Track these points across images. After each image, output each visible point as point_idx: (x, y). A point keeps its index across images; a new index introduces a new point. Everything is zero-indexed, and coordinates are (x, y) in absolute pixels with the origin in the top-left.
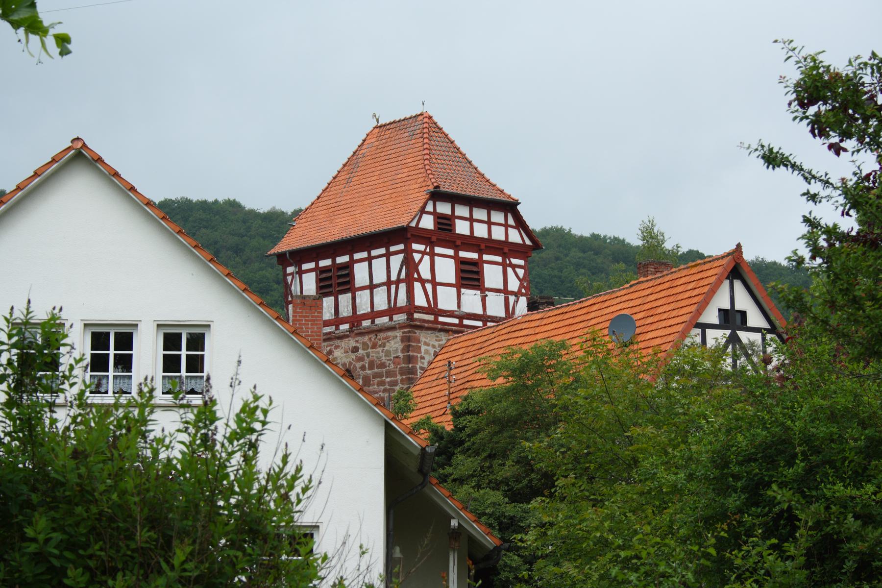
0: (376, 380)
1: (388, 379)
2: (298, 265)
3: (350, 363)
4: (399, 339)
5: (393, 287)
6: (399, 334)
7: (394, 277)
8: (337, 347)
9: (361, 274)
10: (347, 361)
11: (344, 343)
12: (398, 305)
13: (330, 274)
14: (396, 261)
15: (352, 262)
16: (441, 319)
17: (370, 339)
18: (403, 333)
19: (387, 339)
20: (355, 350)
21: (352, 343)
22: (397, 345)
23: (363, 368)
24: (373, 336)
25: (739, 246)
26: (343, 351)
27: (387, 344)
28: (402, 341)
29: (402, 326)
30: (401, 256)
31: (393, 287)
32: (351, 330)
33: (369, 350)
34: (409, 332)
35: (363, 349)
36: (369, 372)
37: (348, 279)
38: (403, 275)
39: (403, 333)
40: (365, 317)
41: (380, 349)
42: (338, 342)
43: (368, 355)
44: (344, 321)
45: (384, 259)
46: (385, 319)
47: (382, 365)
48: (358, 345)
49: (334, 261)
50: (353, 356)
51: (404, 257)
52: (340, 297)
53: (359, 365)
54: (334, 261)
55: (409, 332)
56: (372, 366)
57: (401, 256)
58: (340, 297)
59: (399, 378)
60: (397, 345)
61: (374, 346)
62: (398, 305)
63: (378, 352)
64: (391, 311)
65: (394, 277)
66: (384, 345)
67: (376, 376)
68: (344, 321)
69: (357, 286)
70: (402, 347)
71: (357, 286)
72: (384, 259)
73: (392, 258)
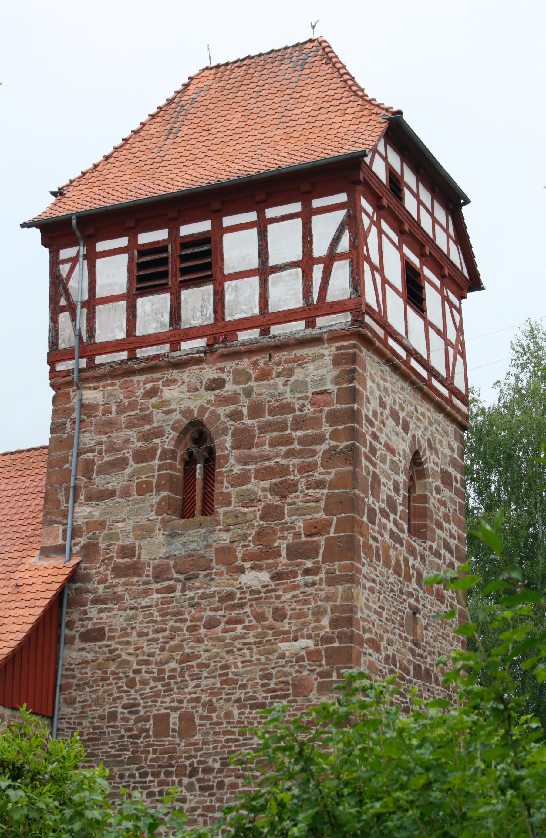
0: (268, 437)
1: (299, 433)
2: (90, 241)
3: (202, 409)
4: (328, 360)
5: (318, 271)
6: (328, 351)
7: (320, 249)
8: (169, 383)
9: (238, 249)
10: (194, 405)
11: (187, 375)
12: (331, 297)
13: (316, 578)
14: (325, 227)
15: (219, 231)
16: (99, 360)
17: (255, 364)
18: (338, 348)
19: (300, 362)
20: (216, 384)
21: (209, 372)
22: (322, 371)
23: (236, 416)
24: (262, 360)
25: (483, 289)
26: (185, 388)
27: (298, 370)
28: (336, 362)
29: (335, 336)
30: (341, 214)
31: (318, 271)
32: (209, 349)
33: (251, 383)
34: (354, 346)
35: (236, 382)
36: (250, 422)
37: (206, 248)
38: (344, 245)
39: (338, 348)
40: (245, 324)
41: (280, 381)
42: (175, 373)
43: (248, 393)
44: (193, 333)
45: (298, 222)
46: (253, 334)
47: (287, 408)
48: (224, 376)
49: (174, 232)
50: (211, 396)
51: (348, 216)
52: (185, 294)
53: (222, 411)
54: (174, 232)
55: (354, 346)
56: (256, 410)
57: (341, 214)
58: (185, 294)
59: (327, 429)
60: (322, 371)
61: (264, 375)
62: (331, 297)
63: (276, 386)
64: (309, 313)
65: (320, 249)
66: (290, 373)
67: (265, 428)
68: (193, 333)
69: (227, 271)
70: (335, 373)
71: (227, 271)
72: (298, 222)
73: (317, 221)
